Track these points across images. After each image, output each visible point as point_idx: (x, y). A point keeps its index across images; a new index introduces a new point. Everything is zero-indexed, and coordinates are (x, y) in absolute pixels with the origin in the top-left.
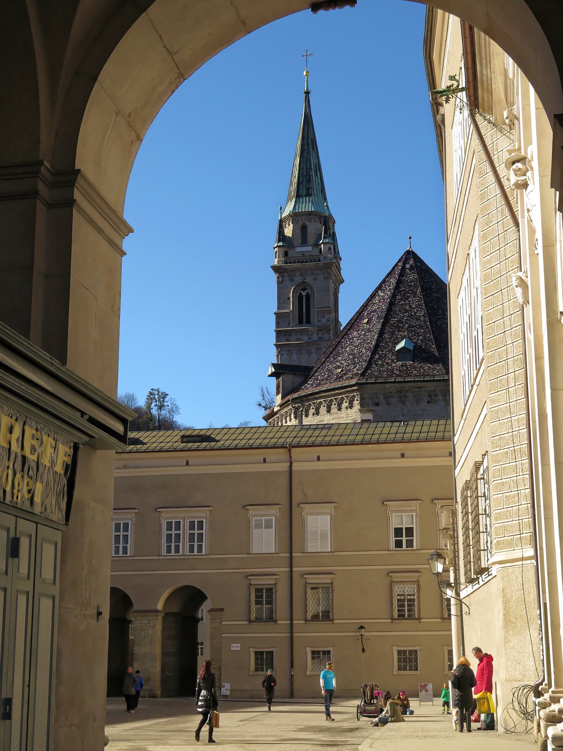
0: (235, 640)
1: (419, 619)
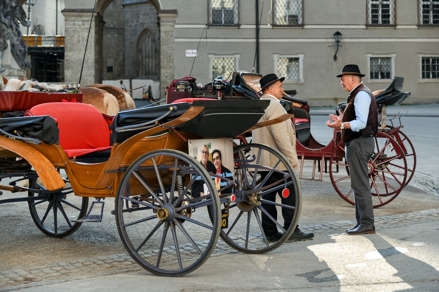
0: (190, 46)
1: (395, 25)
